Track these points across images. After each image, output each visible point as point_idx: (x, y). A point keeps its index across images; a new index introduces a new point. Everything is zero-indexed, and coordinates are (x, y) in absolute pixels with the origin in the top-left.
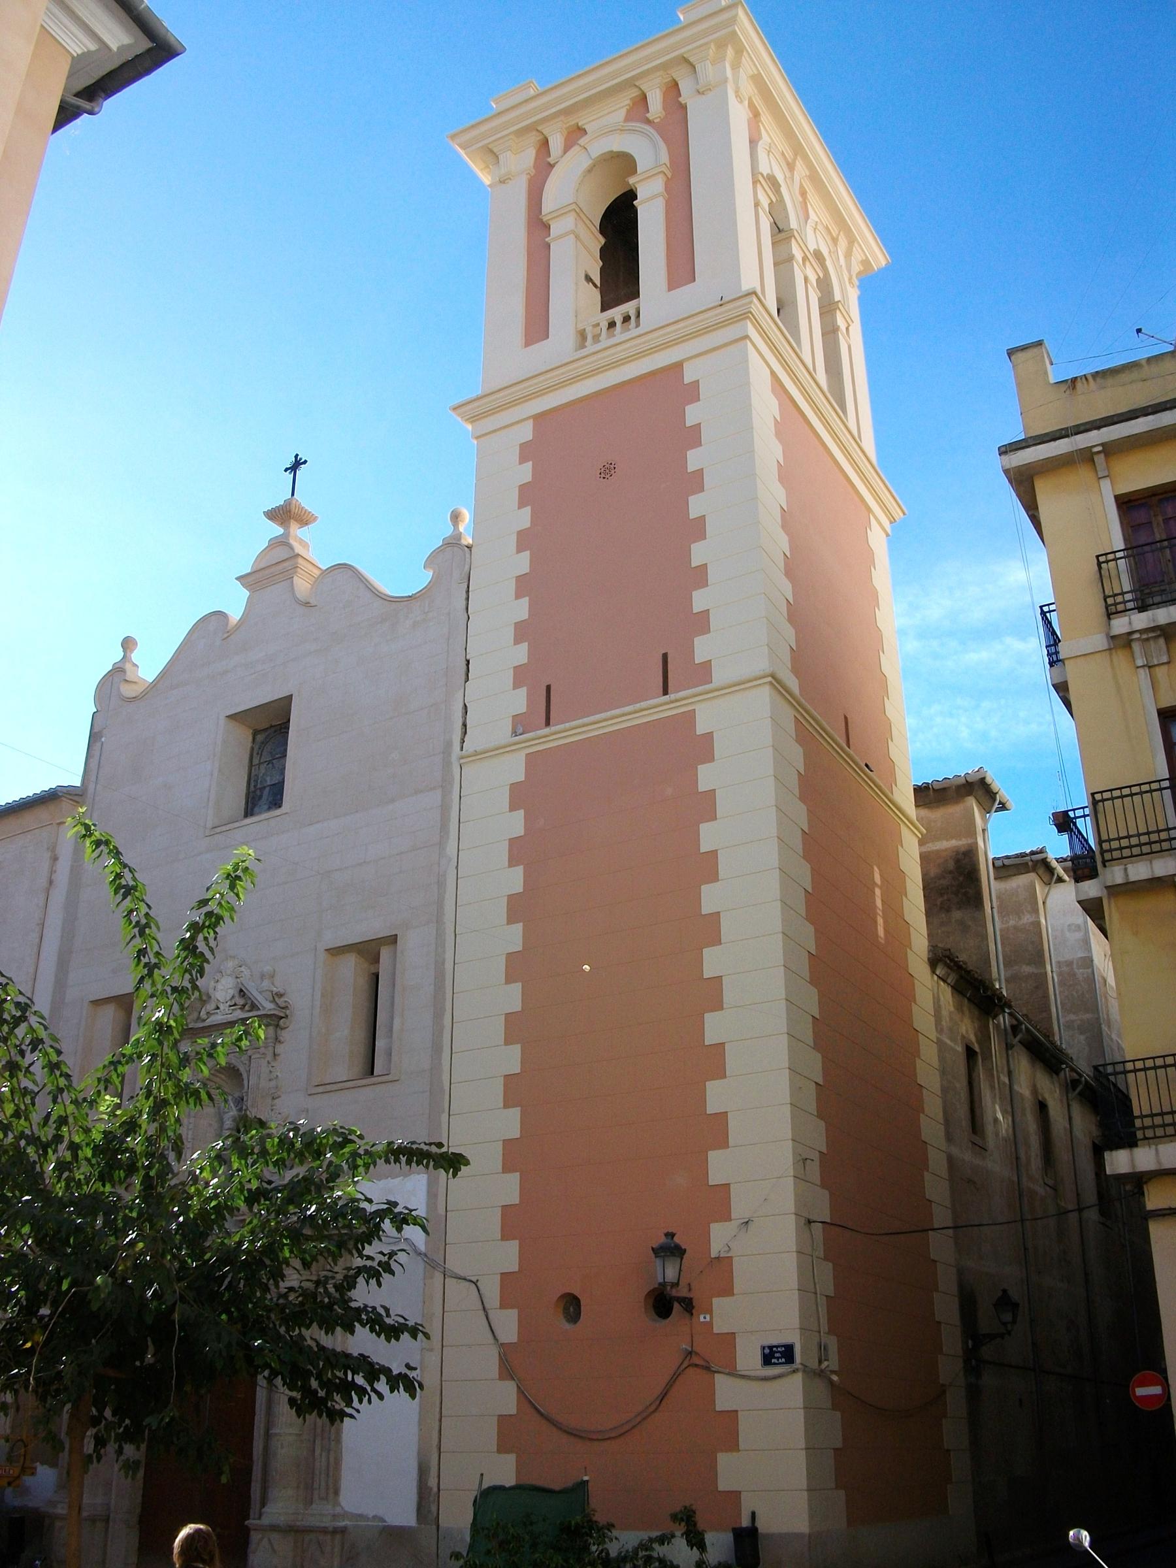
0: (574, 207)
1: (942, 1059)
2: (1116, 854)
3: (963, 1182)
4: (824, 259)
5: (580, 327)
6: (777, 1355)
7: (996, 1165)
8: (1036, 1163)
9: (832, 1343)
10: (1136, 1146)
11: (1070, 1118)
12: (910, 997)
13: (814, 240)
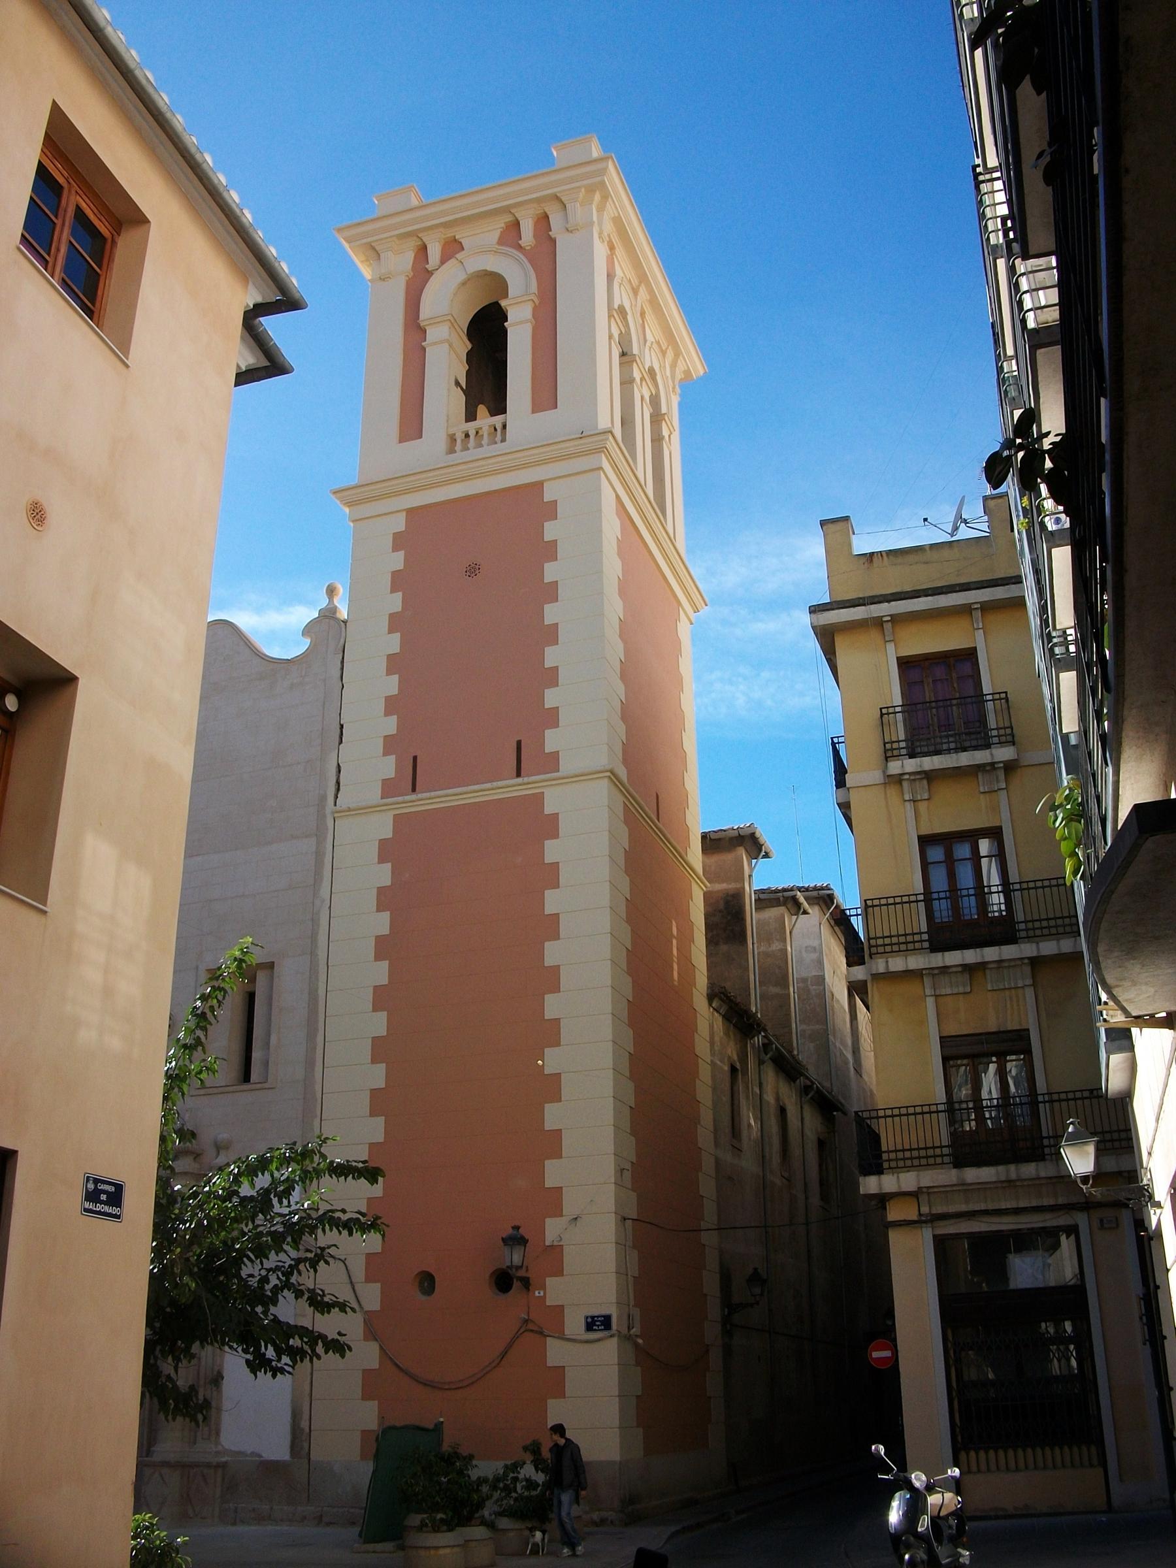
0: (450, 317)
1: (713, 1077)
2: (881, 949)
3: (727, 1178)
4: (626, 313)
5: (451, 431)
7: (748, 1163)
8: (776, 1159)
9: (636, 1313)
10: (882, 1173)
11: (802, 1118)
12: (692, 1029)
13: (650, 358)
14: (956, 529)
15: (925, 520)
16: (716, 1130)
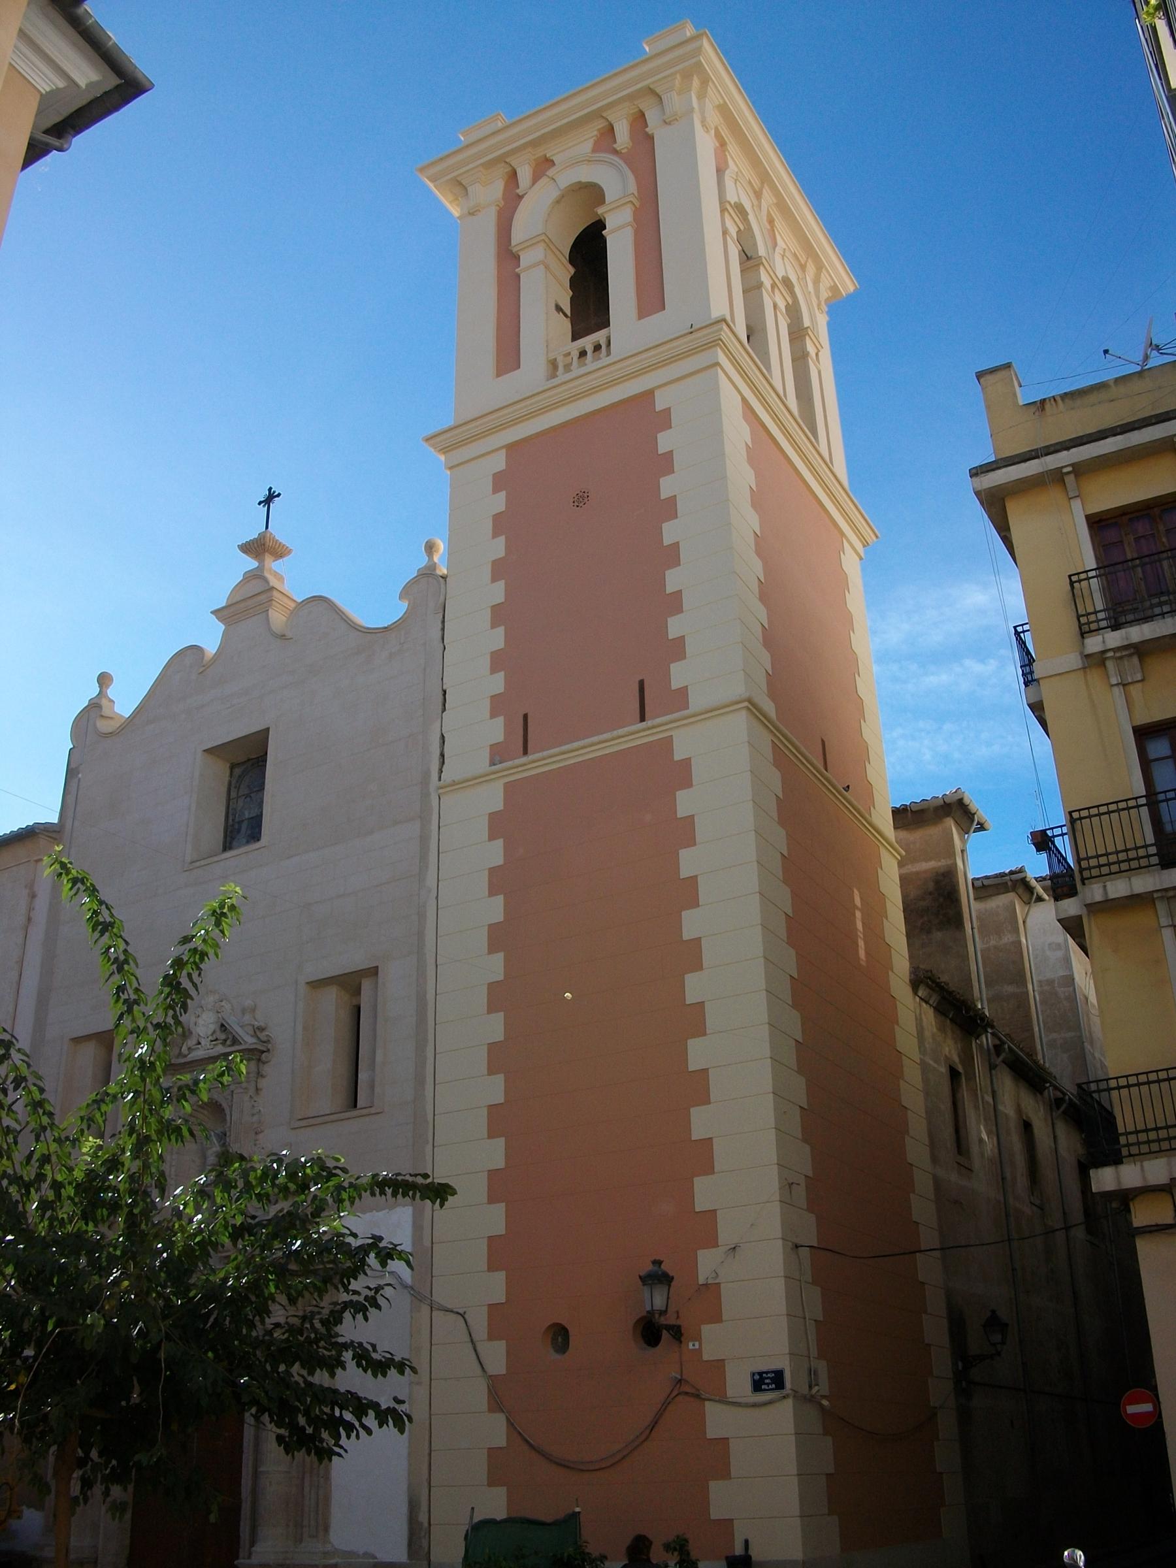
0: (543, 237)
1: (926, 1081)
2: (1095, 872)
3: (949, 1202)
4: (747, 214)
6: (767, 1381)
7: (981, 1185)
8: (1022, 1182)
9: (822, 1366)
11: (1055, 1137)
14: (1146, 358)
15: (1106, 352)
16: (933, 1144)
